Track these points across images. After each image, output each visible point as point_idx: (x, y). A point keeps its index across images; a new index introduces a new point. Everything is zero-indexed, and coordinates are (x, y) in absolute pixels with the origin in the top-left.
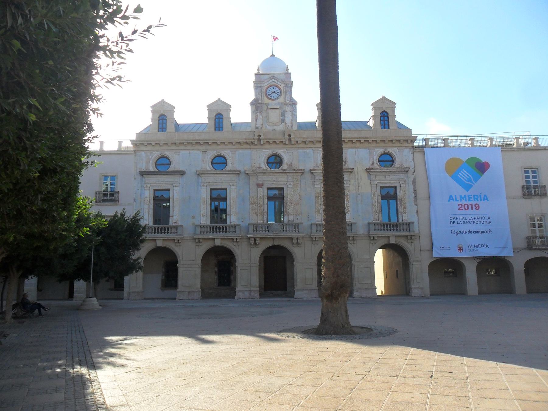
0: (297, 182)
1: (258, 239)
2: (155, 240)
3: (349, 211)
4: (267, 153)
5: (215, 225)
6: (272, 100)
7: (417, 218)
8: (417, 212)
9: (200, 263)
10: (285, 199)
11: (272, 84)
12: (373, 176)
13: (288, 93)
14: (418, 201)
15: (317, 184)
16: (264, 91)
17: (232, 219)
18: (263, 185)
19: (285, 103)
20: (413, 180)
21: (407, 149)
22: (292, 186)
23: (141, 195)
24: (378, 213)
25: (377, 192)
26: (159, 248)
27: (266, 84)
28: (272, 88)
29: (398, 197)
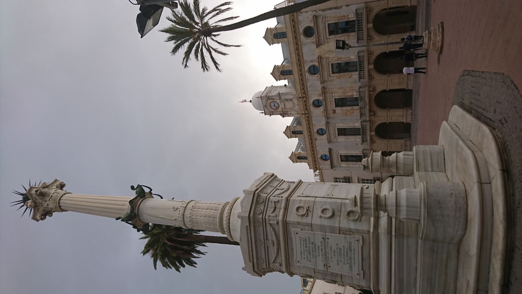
0: (330, 91)
1: (369, 78)
2: (369, 69)
3: (349, 57)
4: (308, 75)
5: (356, 30)
6: (279, 106)
7: (352, 5)
8: (347, 6)
9: (386, 75)
10: (342, 97)
11: (269, 106)
12: (322, 42)
13: (273, 98)
14: (338, 6)
15: (330, 79)
16: (274, 111)
17: (358, 125)
18: (334, 110)
19: (280, 99)
20: (322, 11)
21: (299, 17)
22: (333, 94)
23: (344, 167)
24: (349, 37)
25: (333, 38)
26: (374, 66)
27: (270, 110)
28: (272, 106)
29: (336, 21)
